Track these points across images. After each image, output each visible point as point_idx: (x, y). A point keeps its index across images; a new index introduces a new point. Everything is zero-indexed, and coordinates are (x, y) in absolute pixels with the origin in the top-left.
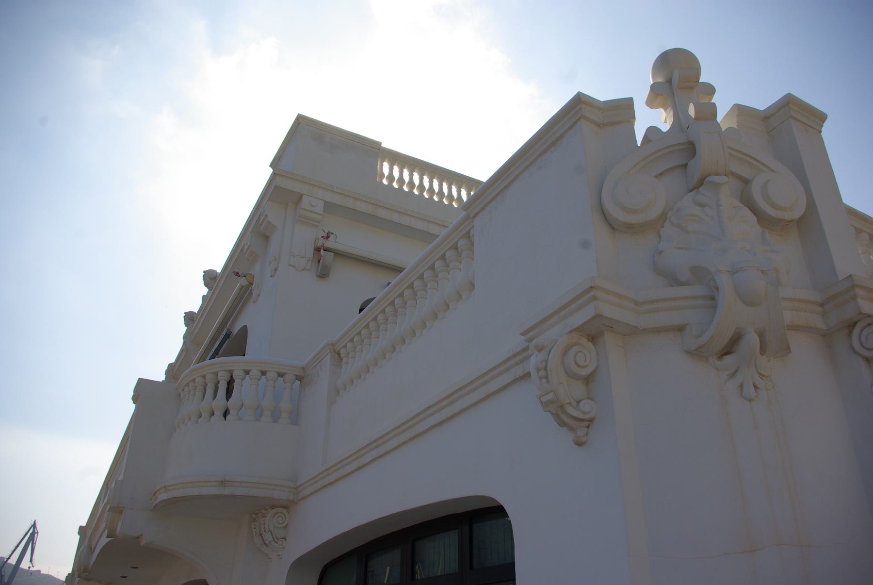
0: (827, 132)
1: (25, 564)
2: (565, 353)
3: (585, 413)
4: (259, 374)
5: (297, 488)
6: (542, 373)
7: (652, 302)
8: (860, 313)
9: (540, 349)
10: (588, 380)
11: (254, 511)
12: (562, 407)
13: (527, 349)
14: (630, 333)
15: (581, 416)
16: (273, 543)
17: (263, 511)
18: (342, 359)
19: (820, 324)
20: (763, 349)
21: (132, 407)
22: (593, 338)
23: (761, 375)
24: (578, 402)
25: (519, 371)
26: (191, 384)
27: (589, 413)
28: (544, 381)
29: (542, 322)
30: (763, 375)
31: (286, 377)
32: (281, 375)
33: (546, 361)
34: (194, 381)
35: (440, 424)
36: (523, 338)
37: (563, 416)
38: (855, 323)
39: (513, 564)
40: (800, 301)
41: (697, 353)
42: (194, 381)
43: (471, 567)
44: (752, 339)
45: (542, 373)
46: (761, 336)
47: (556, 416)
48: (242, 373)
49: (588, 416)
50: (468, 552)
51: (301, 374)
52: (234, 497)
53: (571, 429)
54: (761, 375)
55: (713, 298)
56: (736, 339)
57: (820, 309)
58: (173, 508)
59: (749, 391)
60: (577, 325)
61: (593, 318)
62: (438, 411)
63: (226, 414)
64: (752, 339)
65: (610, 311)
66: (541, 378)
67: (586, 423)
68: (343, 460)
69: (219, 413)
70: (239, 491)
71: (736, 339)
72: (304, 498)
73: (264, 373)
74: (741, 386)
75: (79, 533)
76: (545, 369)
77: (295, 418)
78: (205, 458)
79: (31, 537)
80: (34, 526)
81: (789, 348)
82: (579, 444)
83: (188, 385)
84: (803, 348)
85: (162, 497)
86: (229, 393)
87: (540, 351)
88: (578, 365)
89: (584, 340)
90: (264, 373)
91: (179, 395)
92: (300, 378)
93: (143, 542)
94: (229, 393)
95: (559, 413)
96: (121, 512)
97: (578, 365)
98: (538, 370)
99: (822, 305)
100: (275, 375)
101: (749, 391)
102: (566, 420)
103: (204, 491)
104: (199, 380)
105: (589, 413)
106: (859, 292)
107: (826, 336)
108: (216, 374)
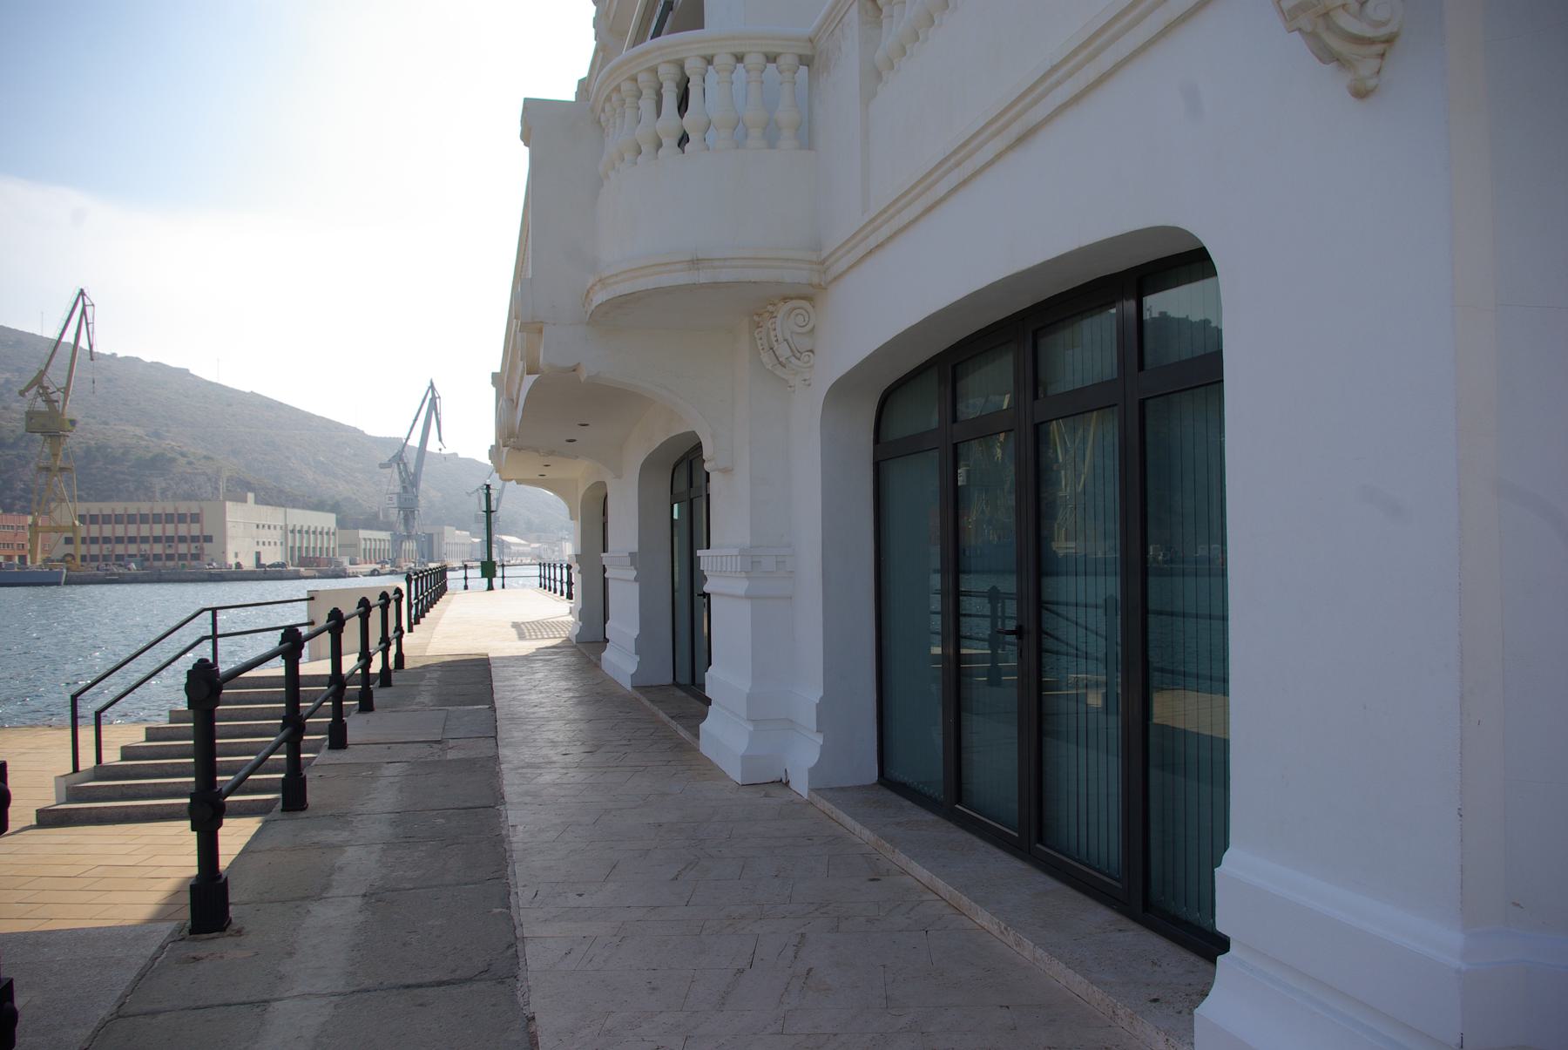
1: (433, 446)
4: (731, 60)
5: (823, 263)
11: (758, 308)
15: (1369, 32)
16: (793, 360)
17: (770, 308)
18: (881, 10)
21: (524, 152)
26: (614, 97)
27: (1384, 24)
31: (781, 61)
32: (771, 58)
34: (618, 89)
35: (1076, 99)
39: (1221, 351)
42: (618, 89)
43: (1141, 367)
47: (1312, 37)
48: (700, 64)
49: (1383, 32)
51: (808, 52)
52: (715, 285)
58: (619, 314)
62: (1070, 75)
63: (684, 140)
67: (1379, 48)
68: (897, 200)
69: (670, 142)
70: (725, 275)
72: (840, 276)
73: (739, 58)
75: (494, 383)
77: (807, 137)
78: (659, 223)
79: (432, 404)
80: (432, 387)
82: (1361, 94)
83: (609, 99)
85: (600, 297)
86: (683, 104)
90: (739, 58)
91: (599, 122)
92: (805, 61)
93: (583, 376)
94: (683, 104)
96: (540, 331)
100: (761, 59)
102: (1335, 43)
103: (667, 280)
104: (626, 87)
105: (1384, 24)
108: (654, 71)
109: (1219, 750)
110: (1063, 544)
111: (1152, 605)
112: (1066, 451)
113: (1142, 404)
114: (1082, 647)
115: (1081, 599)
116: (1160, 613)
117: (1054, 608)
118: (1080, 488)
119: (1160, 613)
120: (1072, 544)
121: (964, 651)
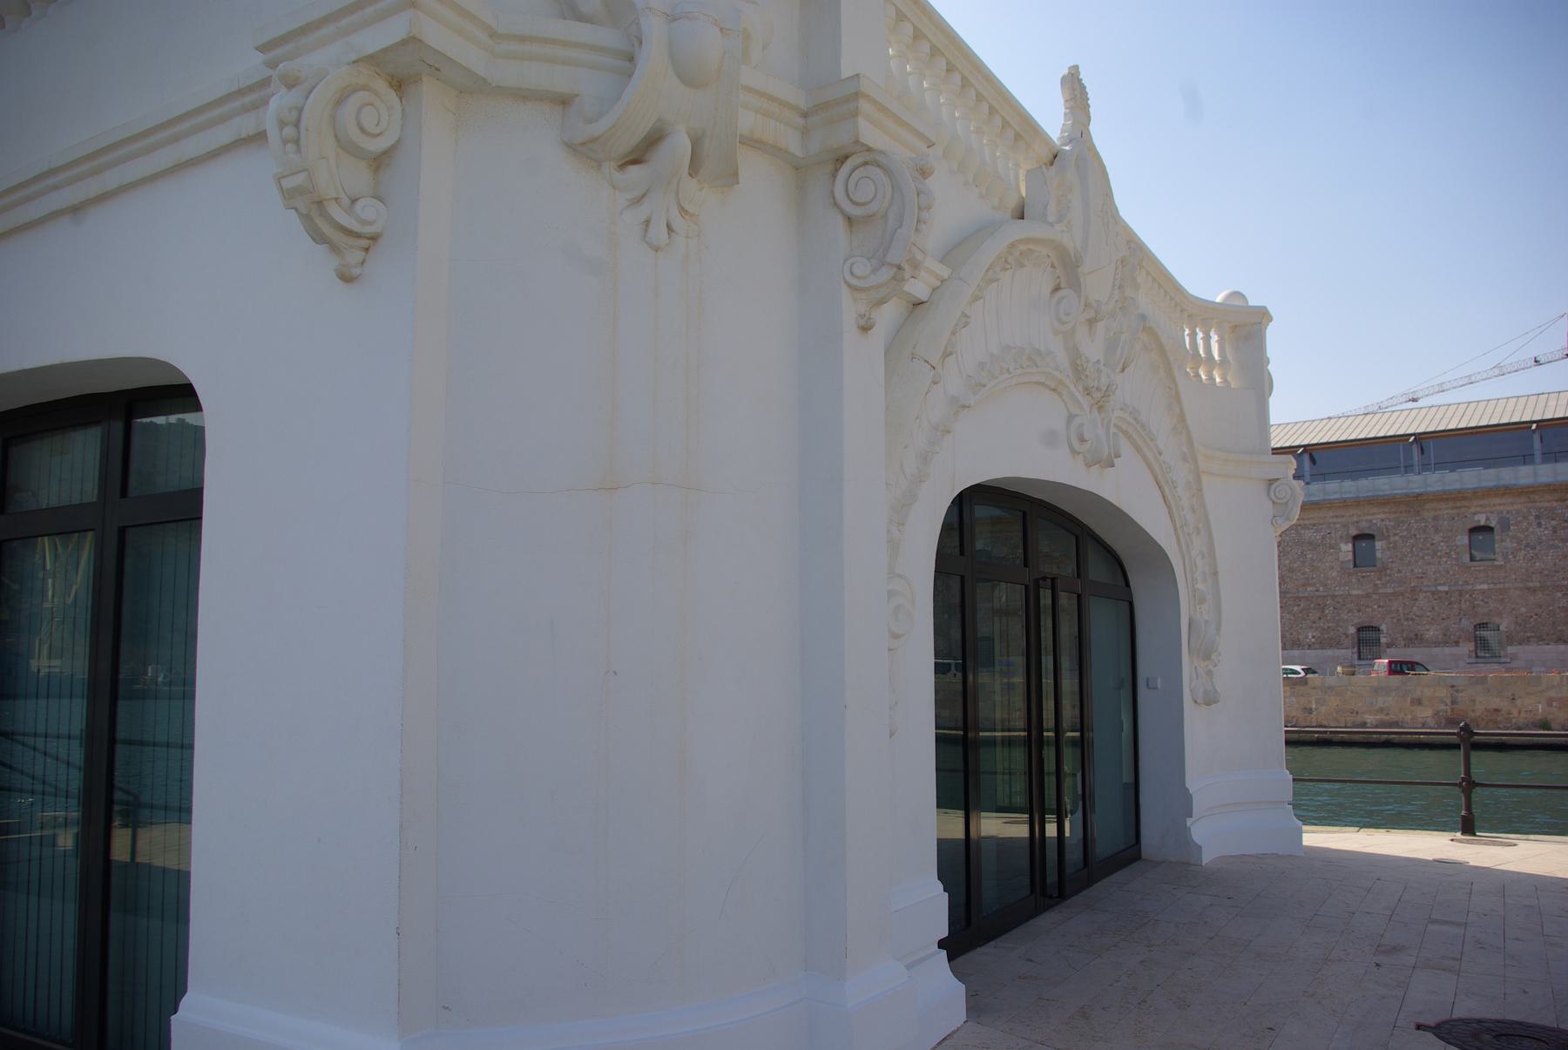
0: (1273, 335)
2: (340, 101)
3: (365, 223)
6: (289, 131)
7: (522, 39)
8: (857, 142)
9: (291, 83)
10: (379, 162)
12: (320, 203)
13: (265, 83)
14: (472, 88)
15: (357, 228)
19: (793, 144)
20: (695, 167)
22: (400, 85)
23: (683, 211)
24: (354, 201)
25: (246, 125)
27: (370, 223)
28: (290, 147)
29: (304, 31)
30: (686, 212)
33: (301, 110)
36: (260, 57)
37: (320, 222)
38: (847, 157)
39: (202, 489)
40: (771, 98)
41: (584, 151)
44: (679, 145)
45: (289, 131)
46: (696, 144)
47: (307, 219)
49: (368, 230)
50: (119, 468)
53: (335, 249)
54: (683, 211)
55: (631, 59)
56: (654, 140)
57: (801, 121)
59: (659, 233)
60: (370, 51)
61: (404, 43)
64: (679, 145)
65: (437, 37)
66: (285, 142)
67: (365, 243)
71: (654, 140)
74: (647, 222)
76: (297, 124)
81: (736, 175)
82: (347, 278)
84: (760, 182)
87: (290, 86)
88: (362, 130)
89: (381, 85)
95: (313, 212)
97: (362, 130)
98: (282, 124)
99: (805, 115)
101: (659, 233)
105: (370, 223)
106: (864, 105)
107: (800, 169)
109: (181, 879)
110: (45, 662)
111: (121, 734)
112: (56, 557)
113: (122, 531)
114: (62, 785)
115: (41, 729)
116: (130, 742)
117: (30, 741)
118: (70, 600)
119: (130, 742)
120: (57, 663)
121: (1077, 734)
